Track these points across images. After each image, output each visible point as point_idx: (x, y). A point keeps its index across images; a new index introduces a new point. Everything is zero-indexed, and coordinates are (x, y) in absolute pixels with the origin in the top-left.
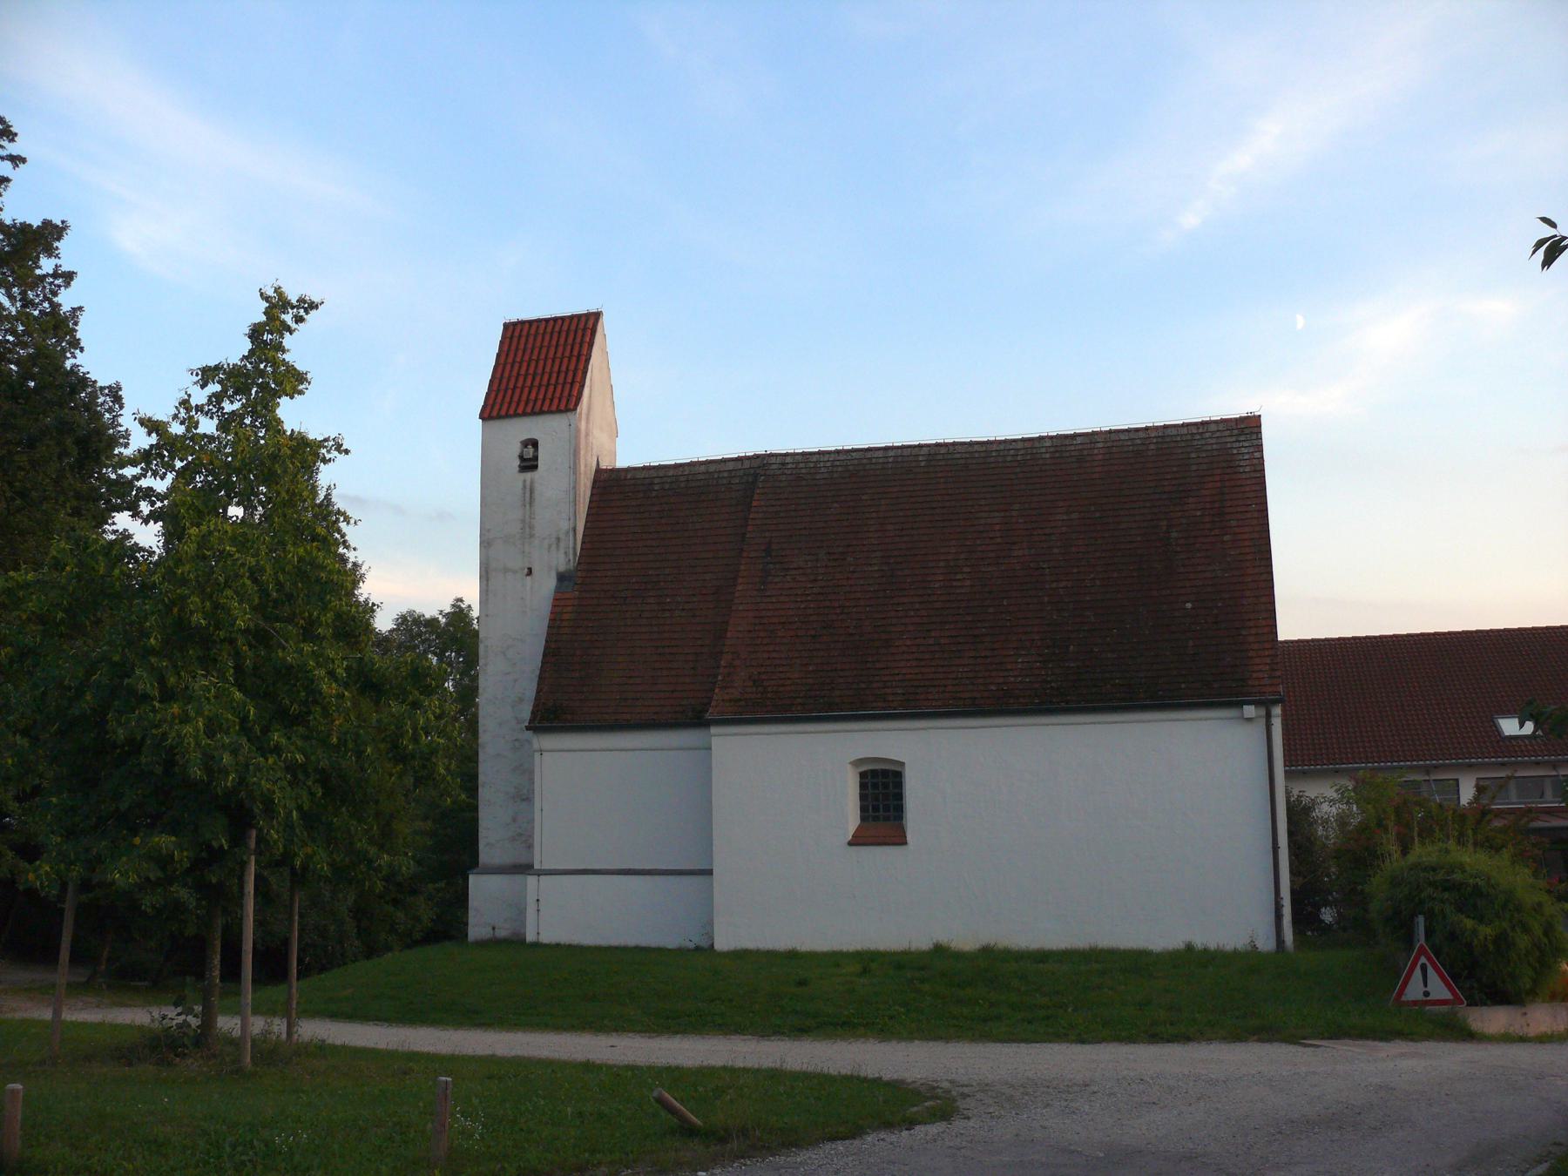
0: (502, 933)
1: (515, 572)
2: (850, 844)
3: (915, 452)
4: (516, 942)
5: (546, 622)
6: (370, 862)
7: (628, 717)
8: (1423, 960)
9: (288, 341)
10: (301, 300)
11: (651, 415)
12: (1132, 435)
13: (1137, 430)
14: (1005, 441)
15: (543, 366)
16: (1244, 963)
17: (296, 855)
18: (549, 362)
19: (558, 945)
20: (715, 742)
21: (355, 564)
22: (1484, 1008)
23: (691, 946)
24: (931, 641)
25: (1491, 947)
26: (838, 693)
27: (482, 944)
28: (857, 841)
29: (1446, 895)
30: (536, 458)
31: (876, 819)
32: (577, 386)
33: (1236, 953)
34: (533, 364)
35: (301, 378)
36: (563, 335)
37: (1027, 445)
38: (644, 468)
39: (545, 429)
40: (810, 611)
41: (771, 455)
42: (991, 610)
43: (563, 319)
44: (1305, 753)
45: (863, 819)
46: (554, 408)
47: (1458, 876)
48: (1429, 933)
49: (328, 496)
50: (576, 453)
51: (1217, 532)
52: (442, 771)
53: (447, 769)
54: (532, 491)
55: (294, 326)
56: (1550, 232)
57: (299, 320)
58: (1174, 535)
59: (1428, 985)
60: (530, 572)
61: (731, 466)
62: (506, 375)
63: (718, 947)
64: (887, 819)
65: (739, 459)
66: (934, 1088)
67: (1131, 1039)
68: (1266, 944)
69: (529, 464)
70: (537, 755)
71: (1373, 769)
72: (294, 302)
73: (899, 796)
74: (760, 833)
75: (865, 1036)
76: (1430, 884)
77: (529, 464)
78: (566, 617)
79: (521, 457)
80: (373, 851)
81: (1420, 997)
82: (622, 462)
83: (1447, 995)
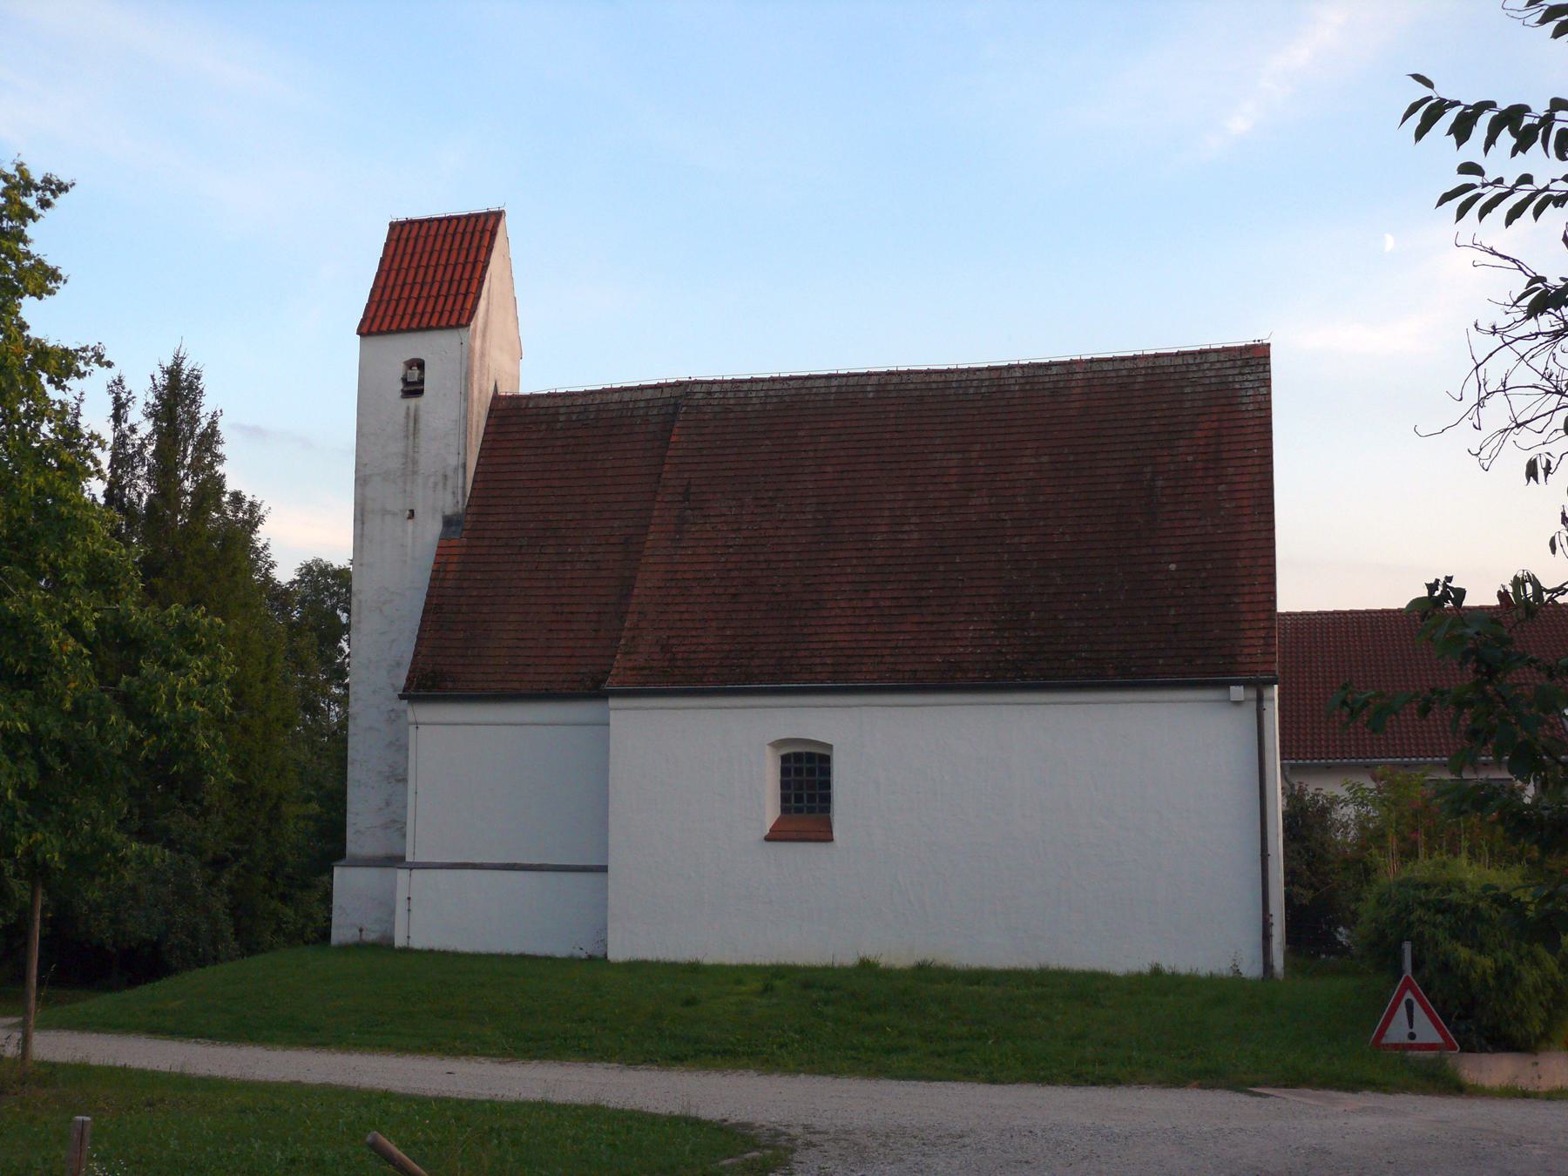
0: (371, 936)
1: (394, 514)
2: (767, 839)
3: (863, 381)
4: (384, 947)
5: (428, 574)
6: (115, 851)
7: (516, 685)
8: (1409, 995)
9: (31, 229)
10: (47, 180)
11: (563, 332)
12: (1117, 365)
13: (1123, 359)
14: (968, 370)
15: (433, 274)
16: (1217, 992)
17: (16, 842)
18: (441, 269)
19: (431, 951)
20: (614, 717)
21: (252, 504)
22: (1484, 1056)
23: (583, 955)
24: (870, 604)
25: (1491, 982)
26: (757, 662)
27: (345, 948)
28: (775, 836)
29: (1439, 918)
30: (422, 382)
31: (799, 810)
32: (471, 297)
33: (1213, 981)
34: (422, 271)
35: (54, 275)
36: (458, 237)
37: (994, 375)
38: (549, 395)
39: (432, 347)
40: (730, 566)
41: (697, 382)
42: (941, 568)
43: (458, 218)
44: (1304, 745)
45: (784, 810)
46: (443, 323)
47: (1455, 896)
48: (1417, 965)
49: (213, 424)
50: (468, 375)
51: (1210, 481)
52: (205, 745)
53: (213, 742)
54: (416, 421)
55: (38, 211)
56: (1425, 92)
57: (45, 204)
58: (1160, 483)
59: (1412, 1025)
60: (412, 514)
61: (649, 394)
62: (390, 283)
63: (610, 957)
64: (811, 810)
65: (658, 387)
66: (778, 1134)
67: (1050, 1081)
68: (1251, 968)
69: (413, 389)
70: (412, 728)
71: (1393, 764)
72: (38, 180)
73: (827, 785)
74: (663, 823)
75: (746, 1067)
76: (1422, 904)
77: (413, 389)
78: (453, 567)
79: (404, 380)
80: (119, 838)
81: (1407, 1041)
82: (525, 389)
83: (1434, 1037)
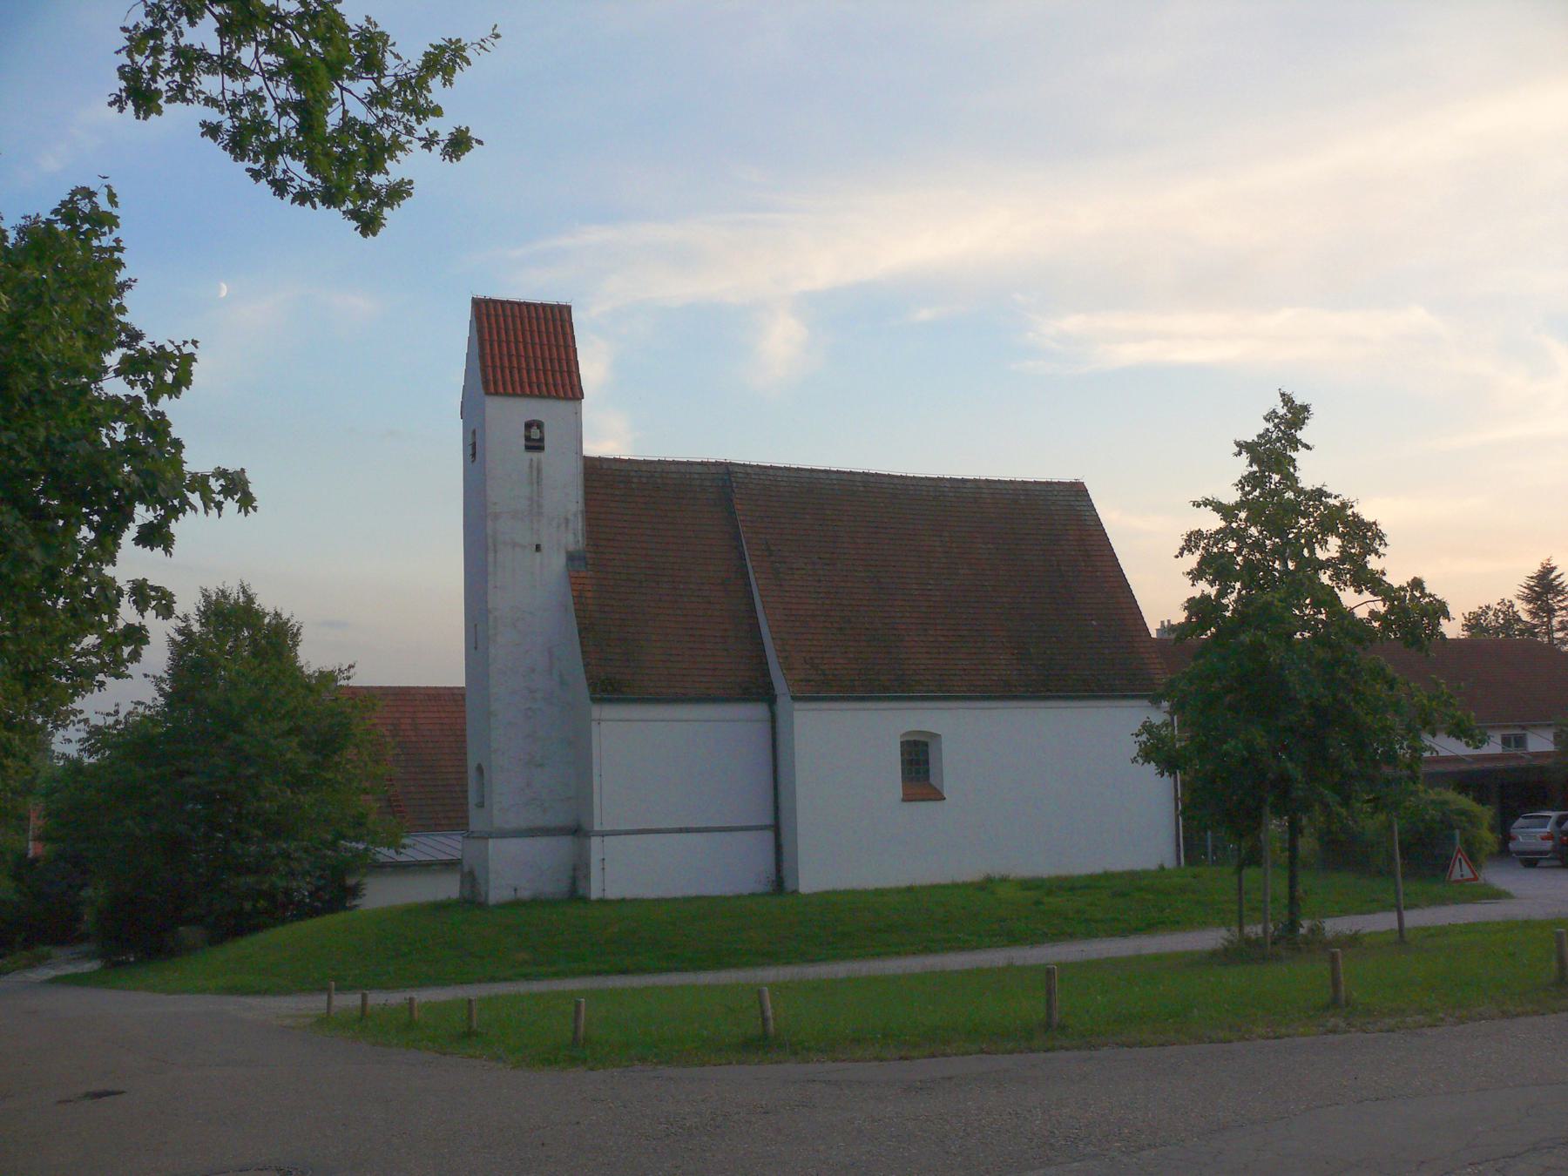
0: (525, 894)
30: (541, 440)
54: (539, 471)
60: (538, 548)
